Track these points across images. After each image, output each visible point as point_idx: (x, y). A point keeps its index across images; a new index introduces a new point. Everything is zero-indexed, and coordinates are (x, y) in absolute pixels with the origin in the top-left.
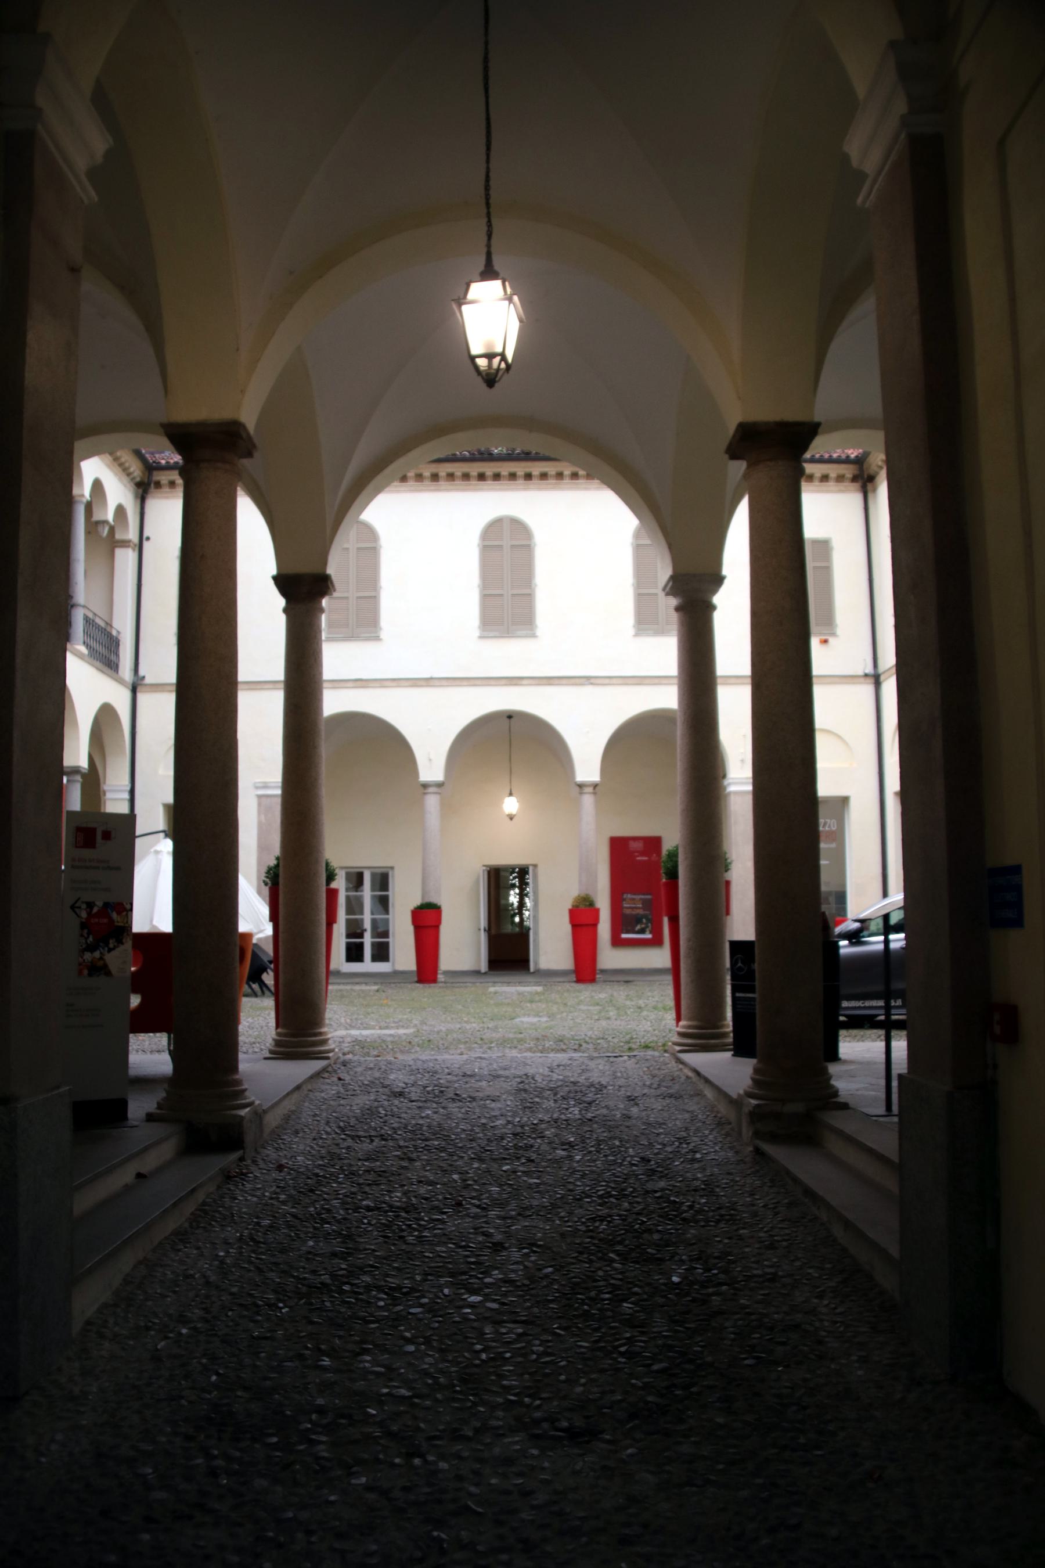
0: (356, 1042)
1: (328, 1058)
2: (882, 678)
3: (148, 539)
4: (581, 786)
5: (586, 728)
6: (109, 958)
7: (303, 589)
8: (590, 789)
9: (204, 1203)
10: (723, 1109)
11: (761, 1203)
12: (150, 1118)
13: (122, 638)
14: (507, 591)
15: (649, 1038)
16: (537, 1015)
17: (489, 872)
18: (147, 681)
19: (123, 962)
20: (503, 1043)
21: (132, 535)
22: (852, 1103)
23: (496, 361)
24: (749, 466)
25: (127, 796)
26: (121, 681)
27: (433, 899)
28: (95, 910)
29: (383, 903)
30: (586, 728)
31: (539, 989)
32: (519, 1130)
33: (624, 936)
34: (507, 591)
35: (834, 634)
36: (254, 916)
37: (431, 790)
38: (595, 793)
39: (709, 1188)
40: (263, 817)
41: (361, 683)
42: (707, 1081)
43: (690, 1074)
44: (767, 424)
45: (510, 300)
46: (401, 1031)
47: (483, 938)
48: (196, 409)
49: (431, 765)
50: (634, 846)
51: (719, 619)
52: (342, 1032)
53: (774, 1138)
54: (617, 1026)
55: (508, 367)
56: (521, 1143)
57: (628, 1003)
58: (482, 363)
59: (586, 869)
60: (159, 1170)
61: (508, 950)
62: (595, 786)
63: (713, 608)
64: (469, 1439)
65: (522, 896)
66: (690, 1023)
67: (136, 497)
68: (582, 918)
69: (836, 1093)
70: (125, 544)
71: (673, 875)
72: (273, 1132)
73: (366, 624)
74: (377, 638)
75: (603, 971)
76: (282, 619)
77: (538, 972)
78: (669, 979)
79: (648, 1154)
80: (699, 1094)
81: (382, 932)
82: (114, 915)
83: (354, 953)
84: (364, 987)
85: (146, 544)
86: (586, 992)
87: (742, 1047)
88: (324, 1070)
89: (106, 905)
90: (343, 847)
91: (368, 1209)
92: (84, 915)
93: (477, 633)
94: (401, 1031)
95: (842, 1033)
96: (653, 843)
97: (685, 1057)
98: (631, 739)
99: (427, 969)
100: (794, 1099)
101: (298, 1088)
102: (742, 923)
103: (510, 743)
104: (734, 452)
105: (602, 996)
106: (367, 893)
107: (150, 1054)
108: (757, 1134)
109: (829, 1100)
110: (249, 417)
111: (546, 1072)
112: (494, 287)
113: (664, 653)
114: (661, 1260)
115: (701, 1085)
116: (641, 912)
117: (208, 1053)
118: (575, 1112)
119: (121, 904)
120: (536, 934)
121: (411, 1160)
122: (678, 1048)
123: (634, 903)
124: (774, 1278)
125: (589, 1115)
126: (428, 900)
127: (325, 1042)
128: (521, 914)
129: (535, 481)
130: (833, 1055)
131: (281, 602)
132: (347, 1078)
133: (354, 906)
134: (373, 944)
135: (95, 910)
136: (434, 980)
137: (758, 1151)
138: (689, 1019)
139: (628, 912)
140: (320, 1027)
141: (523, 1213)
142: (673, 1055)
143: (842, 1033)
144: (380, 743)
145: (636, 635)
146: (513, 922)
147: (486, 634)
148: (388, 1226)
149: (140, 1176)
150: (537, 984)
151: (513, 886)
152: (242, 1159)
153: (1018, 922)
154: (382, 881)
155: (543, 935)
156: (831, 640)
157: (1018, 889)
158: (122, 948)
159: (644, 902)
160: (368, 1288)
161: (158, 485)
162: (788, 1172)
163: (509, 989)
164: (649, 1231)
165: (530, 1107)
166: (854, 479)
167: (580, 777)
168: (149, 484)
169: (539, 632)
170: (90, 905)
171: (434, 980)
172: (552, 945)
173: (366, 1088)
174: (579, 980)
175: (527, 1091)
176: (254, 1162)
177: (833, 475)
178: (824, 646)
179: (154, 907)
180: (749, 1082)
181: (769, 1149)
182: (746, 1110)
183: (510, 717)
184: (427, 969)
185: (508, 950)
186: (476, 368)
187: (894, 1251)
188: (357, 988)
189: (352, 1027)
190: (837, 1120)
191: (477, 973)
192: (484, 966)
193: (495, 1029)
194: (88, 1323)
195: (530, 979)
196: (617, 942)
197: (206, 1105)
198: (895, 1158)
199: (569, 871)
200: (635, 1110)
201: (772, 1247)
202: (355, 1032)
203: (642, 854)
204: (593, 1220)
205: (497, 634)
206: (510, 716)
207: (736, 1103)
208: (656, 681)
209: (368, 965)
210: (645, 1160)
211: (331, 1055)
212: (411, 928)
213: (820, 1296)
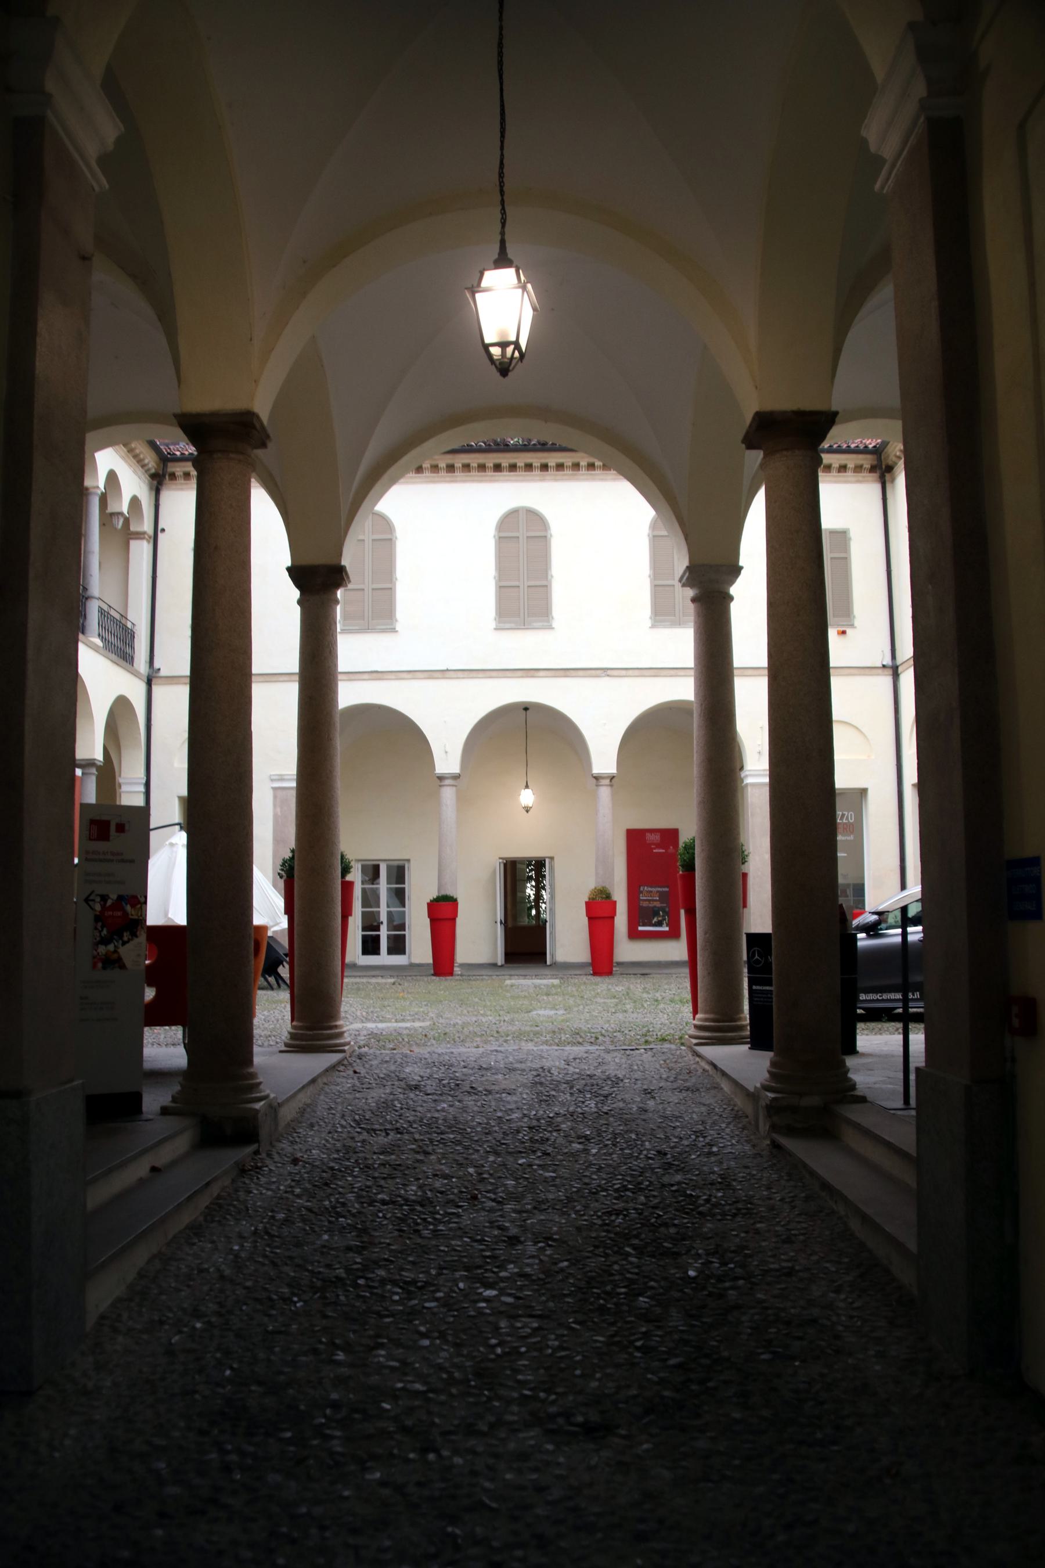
0: (372, 1035)
1: (344, 1051)
2: (900, 669)
3: (163, 530)
4: (597, 778)
5: (603, 720)
7: (318, 581)
8: (607, 782)
9: (219, 1197)
10: (739, 1102)
12: (165, 1111)
13: (136, 630)
14: (523, 582)
15: (665, 1032)
16: (554, 1008)
17: (505, 865)
18: (162, 673)
19: (137, 955)
21: (147, 527)
22: (870, 1096)
23: (510, 350)
25: (142, 789)
26: (136, 674)
27: (450, 892)
28: (109, 903)
29: (399, 896)
30: (603, 720)
31: (556, 982)
32: (535, 1123)
33: (640, 928)
34: (523, 582)
35: (852, 626)
37: (447, 782)
38: (611, 786)
40: (278, 810)
42: (724, 1074)
43: (707, 1067)
44: (784, 413)
46: (417, 1024)
48: (208, 399)
49: (447, 757)
52: (358, 1026)
53: (791, 1131)
54: (633, 1020)
56: (537, 1137)
57: (645, 995)
58: (496, 351)
59: (603, 862)
60: (174, 1164)
61: (525, 944)
62: (612, 778)
63: (731, 598)
65: (538, 888)
66: (707, 1016)
67: (151, 488)
68: (599, 911)
69: (853, 1086)
70: (139, 535)
71: (690, 867)
72: (288, 1124)
73: (381, 616)
74: (393, 630)
75: (619, 964)
77: (554, 965)
78: (686, 971)
80: (717, 1087)
81: (398, 925)
82: (128, 908)
83: (371, 946)
84: (380, 980)
85: (160, 536)
86: (603, 985)
87: (759, 1040)
88: (340, 1063)
89: (120, 898)
90: (359, 839)
91: (384, 1202)
92: (98, 907)
93: (493, 625)
94: (417, 1024)
95: (860, 1026)
97: (701, 1049)
98: (648, 731)
99: (443, 962)
100: (812, 1093)
101: (313, 1081)
102: (759, 915)
103: (525, 735)
104: (751, 442)
105: (620, 988)
106: (383, 885)
107: (165, 1047)
108: (774, 1128)
109: (846, 1092)
110: (263, 407)
111: (563, 1065)
112: (508, 275)
113: (681, 645)
114: (678, 1254)
116: (658, 904)
117: (222, 1047)
118: (592, 1105)
119: (135, 897)
120: (553, 926)
122: (695, 1041)
123: (650, 895)
124: (790, 1273)
125: (606, 1109)
126: (443, 893)
127: (340, 1035)
129: (551, 472)
131: (296, 593)
132: (363, 1072)
133: (370, 899)
134: (389, 937)
135: (109, 903)
136: (451, 973)
137: (776, 1146)
138: (706, 1012)
139: (645, 904)
140: (336, 1020)
141: (539, 1206)
142: (690, 1047)
143: (860, 1026)
145: (653, 626)
147: (502, 625)
149: (154, 1169)
151: (530, 878)
152: (257, 1152)
154: (399, 873)
155: (559, 927)
156: (849, 631)
158: (136, 941)
159: (661, 894)
160: (383, 1282)
161: (173, 476)
162: (805, 1165)
163: (525, 982)
164: (665, 1225)
165: (546, 1100)
166: (873, 469)
167: (596, 770)
168: (164, 476)
170: (104, 898)
172: (568, 938)
173: (382, 1082)
175: (543, 1084)
176: (269, 1155)
177: (851, 465)
178: (842, 637)
180: (767, 1075)
181: (783, 1141)
182: (763, 1103)
183: (526, 709)
184: (443, 962)
185: (525, 944)
187: (912, 1246)
188: (374, 980)
190: (853, 1113)
191: (494, 965)
192: (500, 960)
194: (102, 1317)
195: (547, 972)
196: (634, 934)
197: (221, 1101)
198: (913, 1151)
199: (586, 864)
201: (788, 1241)
202: (370, 1025)
203: (658, 846)
204: (610, 1214)
205: (513, 625)
206: (526, 708)
207: (752, 1096)
208: (672, 672)
209: (384, 958)
210: (661, 1153)
211: (346, 1048)
212: (428, 920)
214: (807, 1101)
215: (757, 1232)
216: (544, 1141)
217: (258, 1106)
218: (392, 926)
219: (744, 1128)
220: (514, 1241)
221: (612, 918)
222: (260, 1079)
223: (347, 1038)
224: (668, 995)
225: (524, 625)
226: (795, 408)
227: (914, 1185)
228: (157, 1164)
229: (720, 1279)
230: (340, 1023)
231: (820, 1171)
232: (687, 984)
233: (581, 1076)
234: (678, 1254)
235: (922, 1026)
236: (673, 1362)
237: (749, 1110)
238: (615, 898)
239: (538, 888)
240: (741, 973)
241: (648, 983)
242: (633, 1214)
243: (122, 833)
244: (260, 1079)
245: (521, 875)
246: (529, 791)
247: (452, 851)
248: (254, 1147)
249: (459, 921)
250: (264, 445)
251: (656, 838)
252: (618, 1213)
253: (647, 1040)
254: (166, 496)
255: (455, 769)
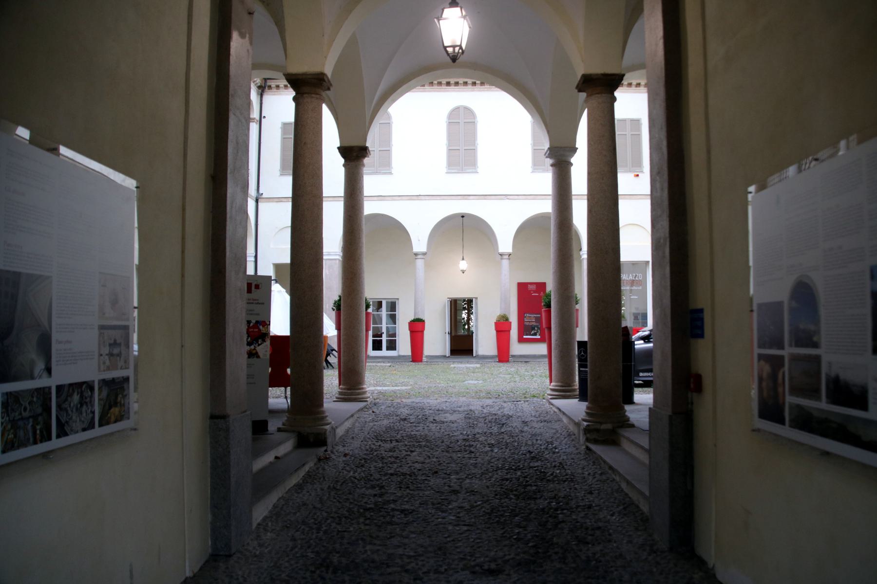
0: (380, 393)
6: (259, 349)
7: (354, 154)
8: (507, 257)
9: (309, 472)
10: (572, 428)
11: (587, 473)
12: (279, 430)
14: (462, 150)
15: (535, 392)
18: (264, 196)
19: (265, 349)
20: (458, 394)
22: (636, 424)
23: (457, 49)
24: (587, 96)
27: (420, 317)
29: (393, 318)
30: (505, 228)
31: (478, 366)
32: (466, 437)
34: (462, 150)
35: (642, 172)
36: (329, 329)
37: (419, 257)
39: (561, 465)
41: (381, 197)
42: (564, 414)
44: (597, 75)
45: (464, 17)
46: (404, 388)
47: (448, 337)
48: (302, 67)
49: (420, 242)
50: (530, 287)
51: (573, 170)
52: (372, 388)
53: (596, 442)
54: (521, 385)
55: (463, 52)
56: (468, 445)
58: (450, 50)
59: (505, 301)
60: (286, 455)
61: (462, 345)
63: (572, 164)
64: (442, 573)
65: (469, 314)
68: (502, 328)
69: (628, 419)
71: (549, 306)
72: (340, 438)
73: (386, 166)
74: (391, 173)
75: (513, 356)
76: (343, 169)
77: (478, 357)
78: (547, 360)
79: (531, 449)
80: (560, 420)
81: (392, 335)
82: (261, 327)
83: (377, 346)
84: (382, 364)
85: (263, 120)
86: (504, 367)
87: (583, 397)
88: (365, 407)
89: (257, 322)
90: (374, 288)
91: (392, 474)
93: (445, 170)
94: (404, 388)
95: (636, 389)
96: (542, 286)
97: (553, 401)
98: (528, 230)
99: (417, 355)
100: (607, 421)
101: (352, 416)
102: (582, 333)
103: (463, 230)
104: (580, 88)
105: (512, 369)
107: (279, 398)
108: (587, 440)
109: (626, 423)
110: (328, 71)
111: (481, 409)
112: (457, 10)
113: (545, 181)
114: (536, 498)
115: (561, 416)
116: (534, 324)
117: (308, 398)
118: (495, 429)
119: (264, 322)
120: (477, 335)
121: (412, 451)
124: (590, 507)
125: (503, 430)
127: (365, 393)
128: (469, 324)
130: (630, 401)
131: (342, 161)
132: (378, 412)
133: (378, 320)
134: (387, 341)
136: (421, 361)
137: (588, 448)
139: (527, 324)
141: (471, 476)
143: (636, 389)
144: (393, 230)
146: (464, 329)
148: (401, 483)
149: (276, 458)
150: (477, 363)
151: (464, 309)
152: (326, 451)
153: (702, 336)
154: (392, 306)
155: (480, 336)
157: (702, 320)
158: (265, 344)
160: (393, 510)
161: (270, 87)
162: (601, 458)
163: (462, 365)
164: (531, 485)
165: (473, 426)
167: (501, 250)
169: (479, 170)
171: (421, 361)
172: (485, 343)
173: (387, 416)
174: (500, 361)
175: (469, 415)
176: (332, 452)
179: (280, 323)
180: (584, 414)
181: (593, 447)
182: (582, 428)
184: (417, 355)
185: (462, 345)
186: (447, 52)
187: (647, 493)
188: (379, 364)
189: (377, 385)
190: (627, 433)
191: (445, 356)
192: (448, 353)
193: (454, 387)
194: (259, 524)
196: (521, 340)
197: (307, 425)
198: (647, 446)
200: (526, 428)
201: (591, 493)
202: (379, 388)
203: (535, 292)
204: (503, 480)
207: (578, 424)
209: (384, 352)
210: (530, 452)
212: (409, 332)
213: (612, 515)
214: (604, 427)
215: (576, 489)
216: (471, 446)
217: (327, 427)
218: (389, 335)
219: (573, 440)
220: (455, 492)
221: (509, 331)
222: (327, 414)
223: (368, 395)
224: (539, 373)
225: (462, 171)
226: (602, 72)
227: (647, 461)
228: (279, 455)
229: (556, 510)
230: (365, 386)
231: (608, 460)
232: (547, 368)
233: (491, 414)
234: (536, 498)
235: (651, 390)
236: (531, 544)
237: (576, 432)
238: (511, 320)
239: (469, 314)
240: (574, 362)
241: (528, 366)
242: (514, 481)
243: (258, 288)
244: (327, 414)
245: (460, 308)
246: (464, 262)
247: (418, 292)
248: (325, 448)
249: (425, 332)
250: (329, 89)
251: (533, 287)
252: (507, 480)
253: (526, 396)
254: (267, 98)
255: (424, 250)
